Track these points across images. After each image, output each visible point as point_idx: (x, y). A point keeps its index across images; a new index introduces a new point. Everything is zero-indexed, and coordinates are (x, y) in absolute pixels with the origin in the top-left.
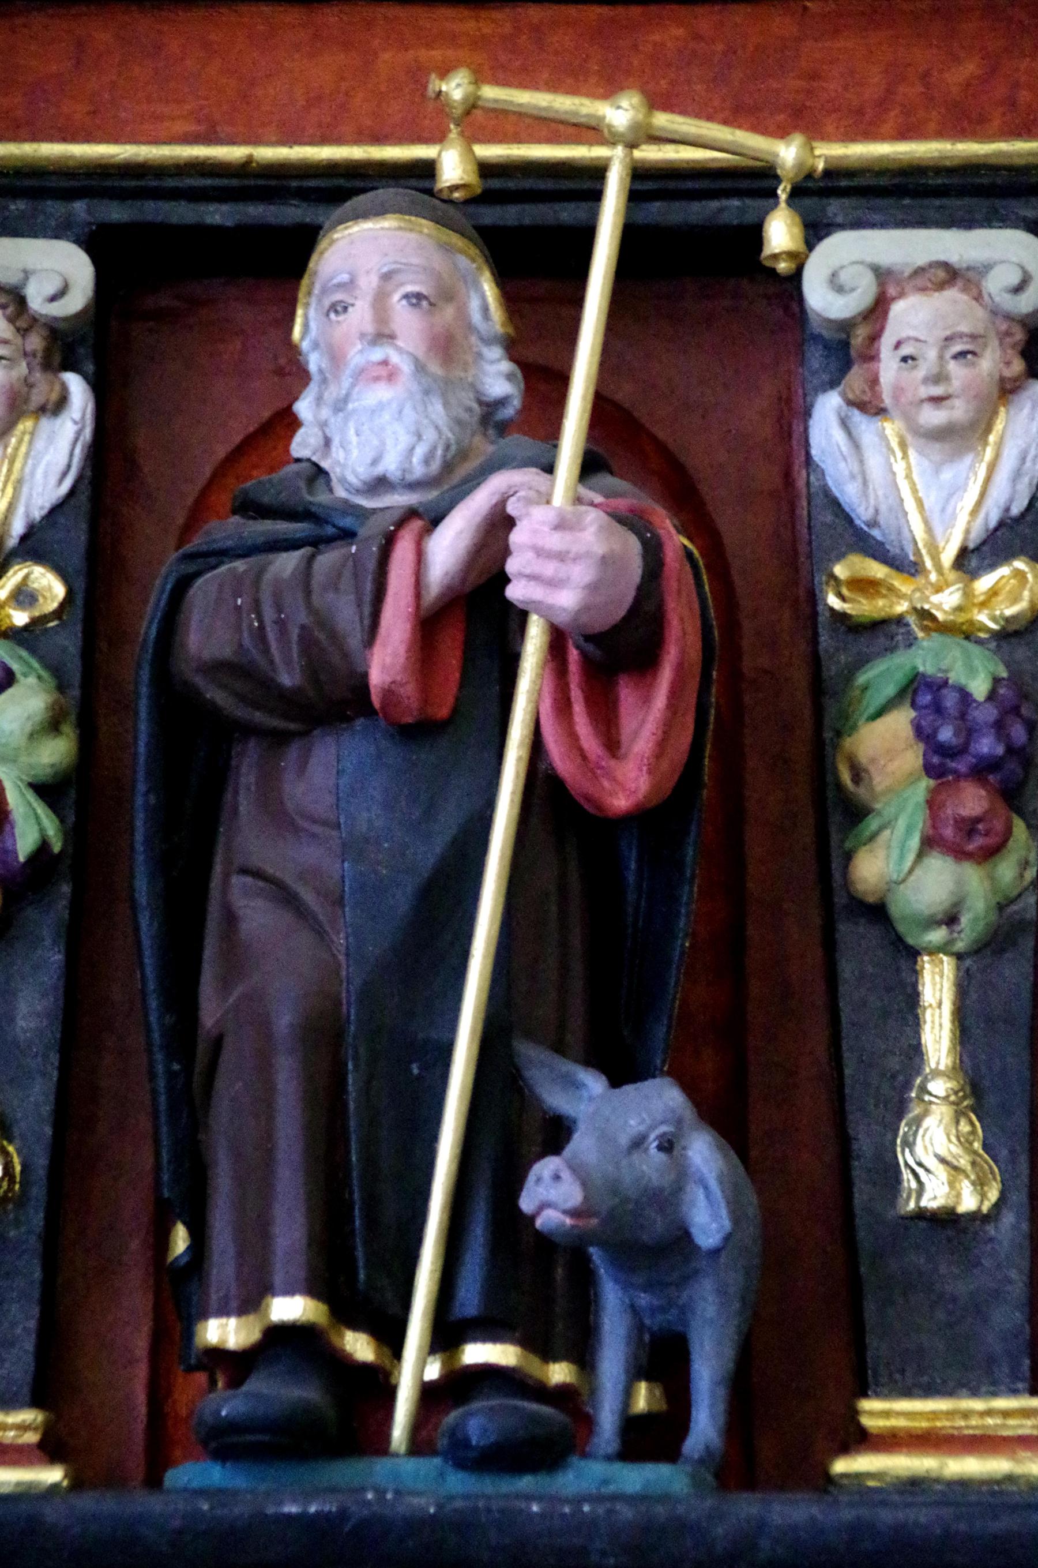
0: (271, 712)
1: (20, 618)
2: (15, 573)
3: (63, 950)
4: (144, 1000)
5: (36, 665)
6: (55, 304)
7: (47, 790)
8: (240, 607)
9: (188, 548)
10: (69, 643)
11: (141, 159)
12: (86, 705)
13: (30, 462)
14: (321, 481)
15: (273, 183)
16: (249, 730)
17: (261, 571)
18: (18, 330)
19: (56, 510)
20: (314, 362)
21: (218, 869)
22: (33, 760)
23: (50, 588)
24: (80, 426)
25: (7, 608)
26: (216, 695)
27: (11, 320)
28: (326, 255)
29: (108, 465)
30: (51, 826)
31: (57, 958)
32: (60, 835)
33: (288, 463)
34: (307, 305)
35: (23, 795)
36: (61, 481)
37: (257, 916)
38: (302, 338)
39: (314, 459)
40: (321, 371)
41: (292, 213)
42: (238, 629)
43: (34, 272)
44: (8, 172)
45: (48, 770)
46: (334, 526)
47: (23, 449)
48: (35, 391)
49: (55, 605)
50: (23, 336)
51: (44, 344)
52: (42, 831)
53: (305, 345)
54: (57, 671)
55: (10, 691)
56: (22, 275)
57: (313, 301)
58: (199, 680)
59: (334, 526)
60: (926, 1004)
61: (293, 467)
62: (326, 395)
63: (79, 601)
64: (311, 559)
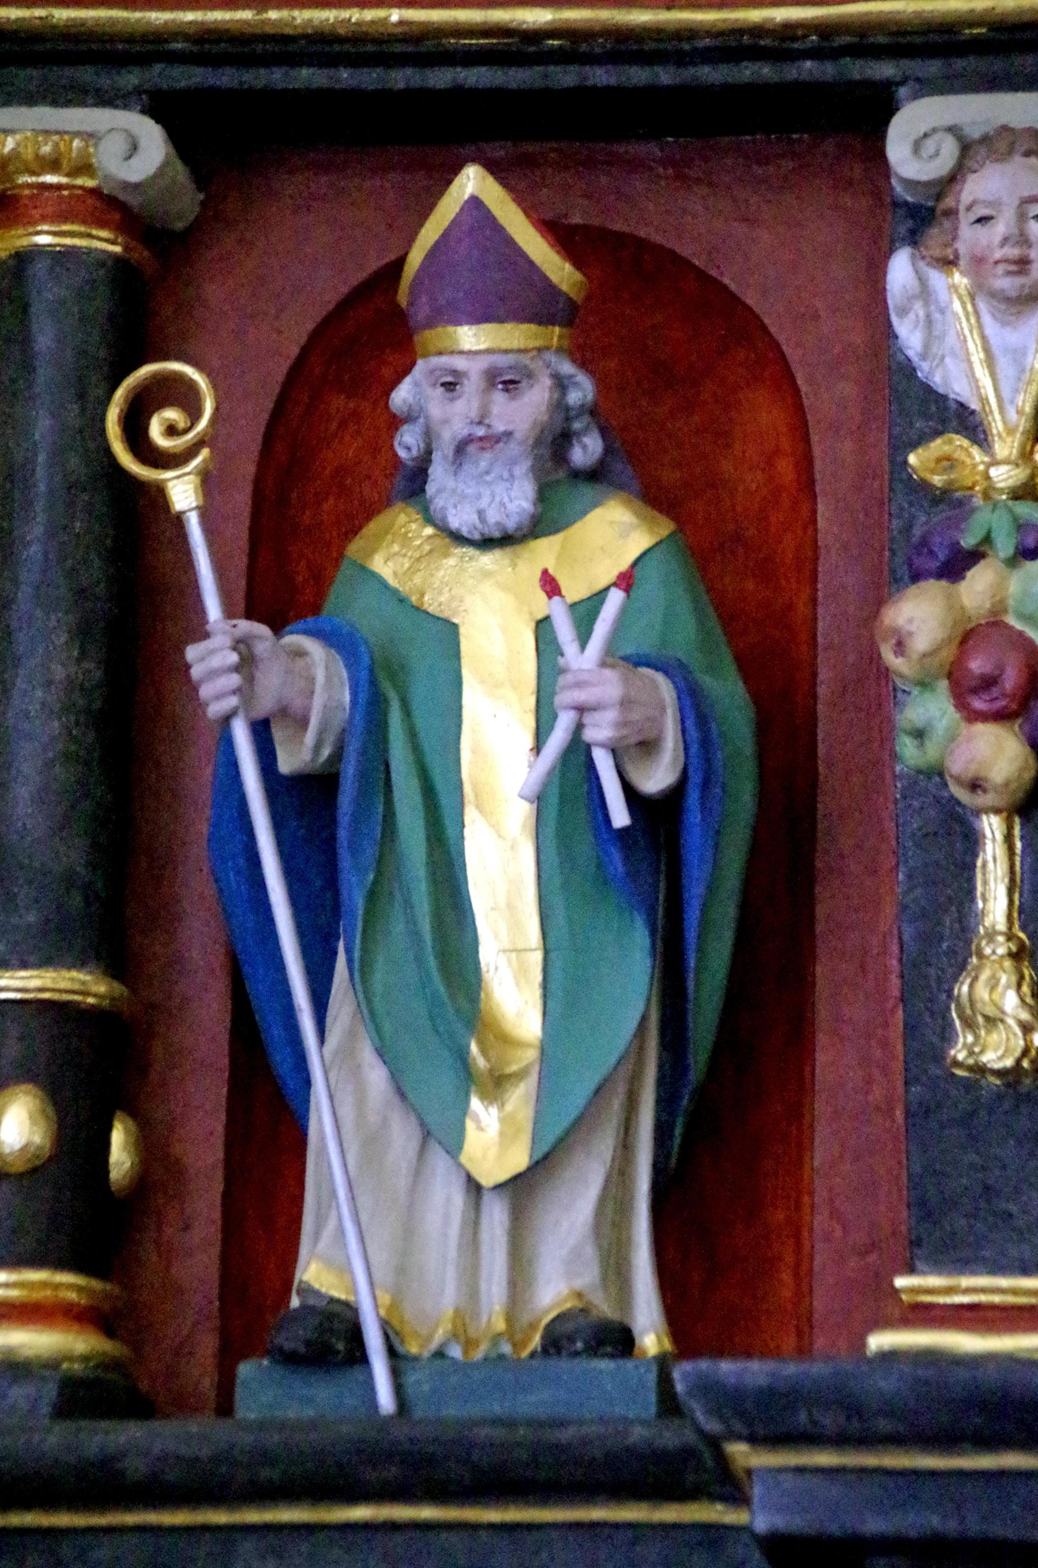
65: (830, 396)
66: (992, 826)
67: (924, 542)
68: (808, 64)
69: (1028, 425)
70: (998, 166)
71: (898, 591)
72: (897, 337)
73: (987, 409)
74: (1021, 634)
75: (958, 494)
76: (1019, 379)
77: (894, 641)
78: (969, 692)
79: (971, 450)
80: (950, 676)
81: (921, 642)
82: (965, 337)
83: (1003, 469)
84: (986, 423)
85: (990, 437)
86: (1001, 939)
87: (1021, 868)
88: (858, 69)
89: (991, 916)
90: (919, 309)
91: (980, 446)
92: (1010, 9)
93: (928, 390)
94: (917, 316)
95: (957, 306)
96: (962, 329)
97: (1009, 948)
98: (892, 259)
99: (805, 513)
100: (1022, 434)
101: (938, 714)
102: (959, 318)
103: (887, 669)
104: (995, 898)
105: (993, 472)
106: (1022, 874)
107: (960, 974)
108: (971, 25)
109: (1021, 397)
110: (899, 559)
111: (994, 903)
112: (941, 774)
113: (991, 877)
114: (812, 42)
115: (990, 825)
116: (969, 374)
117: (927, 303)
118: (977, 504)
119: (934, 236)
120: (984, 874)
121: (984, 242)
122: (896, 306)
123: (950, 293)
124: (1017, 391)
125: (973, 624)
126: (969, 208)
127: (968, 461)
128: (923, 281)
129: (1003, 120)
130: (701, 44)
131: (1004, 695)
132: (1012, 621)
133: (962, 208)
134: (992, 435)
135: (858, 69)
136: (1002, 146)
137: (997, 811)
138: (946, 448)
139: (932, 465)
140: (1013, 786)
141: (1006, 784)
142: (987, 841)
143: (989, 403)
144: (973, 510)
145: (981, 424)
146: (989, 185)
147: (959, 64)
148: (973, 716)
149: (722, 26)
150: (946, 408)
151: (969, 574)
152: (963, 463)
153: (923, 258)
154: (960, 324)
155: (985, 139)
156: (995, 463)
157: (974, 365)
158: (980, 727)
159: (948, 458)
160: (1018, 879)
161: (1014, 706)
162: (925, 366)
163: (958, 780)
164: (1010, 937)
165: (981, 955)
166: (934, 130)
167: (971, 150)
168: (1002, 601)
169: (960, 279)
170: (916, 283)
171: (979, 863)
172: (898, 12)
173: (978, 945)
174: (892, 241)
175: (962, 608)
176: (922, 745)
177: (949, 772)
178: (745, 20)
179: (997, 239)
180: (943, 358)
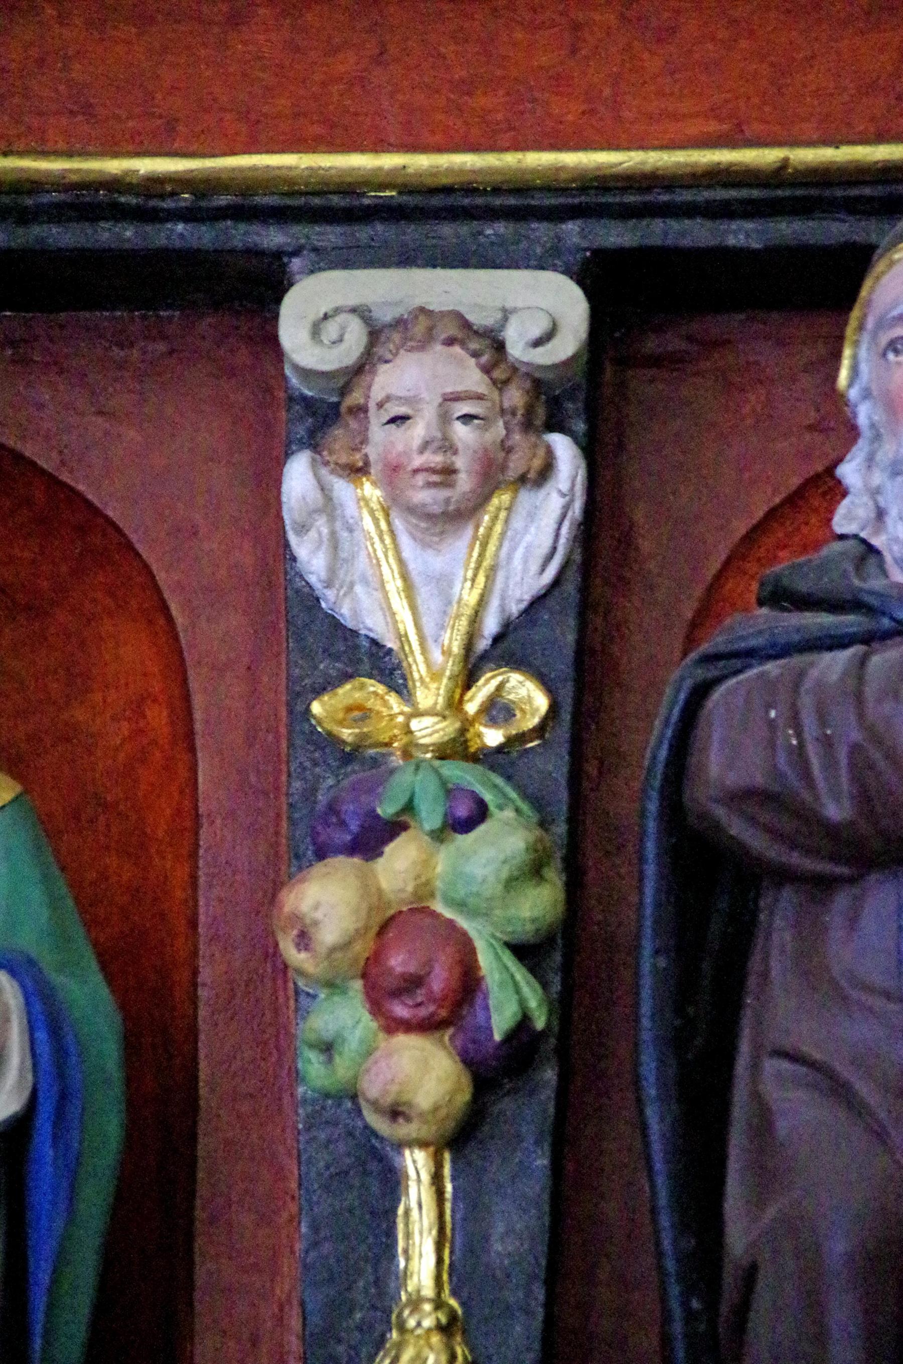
0: (809, 851)
1: (493, 737)
2: (488, 681)
3: (548, 1154)
4: (654, 1221)
5: (513, 795)
6: (540, 350)
7: (526, 952)
8: (773, 720)
9: (705, 648)
10: (555, 766)
11: (648, 168)
12: (576, 849)
13: (374, 561)
14: (872, 560)
15: (814, 192)
16: (784, 876)
17: (801, 675)
18: (494, 382)
19: (538, 601)
20: (864, 414)
21: (745, 1047)
22: (512, 912)
23: (530, 699)
24: (567, 498)
25: (477, 725)
26: (737, 828)
27: (487, 370)
28: (885, 280)
29: (600, 539)
30: (534, 999)
31: (542, 1161)
32: (545, 1010)
33: (826, 542)
34: (856, 344)
35: (498, 958)
36: (543, 569)
37: (797, 1109)
38: (850, 385)
39: (863, 535)
40: (873, 426)
41: (834, 230)
42: (772, 745)
43: (515, 310)
44: (485, 190)
45: (529, 927)
46: (893, 619)
47: (498, 528)
48: (514, 457)
49: (534, 721)
50: (500, 390)
51: (526, 398)
52: (522, 1002)
53: (853, 394)
54: (538, 802)
55: (482, 828)
56: (499, 315)
57: (866, 338)
58: (720, 812)
59: (893, 619)
60: (748, 990)
61: (837, 546)
62: (879, 456)
63: (566, 716)
64: (863, 661)
65: (212, 633)
66: (416, 1164)
67: (332, 808)
68: (180, 227)
69: (456, 668)
70: (415, 356)
71: (300, 869)
72: (294, 559)
73: (407, 648)
74: (451, 923)
75: (372, 751)
76: (445, 612)
77: (295, 932)
78: (386, 994)
79: (387, 697)
80: (364, 976)
81: (329, 935)
82: (377, 559)
83: (428, 721)
84: (405, 664)
85: (410, 683)
86: (427, 1307)
87: (453, 1217)
88: (242, 235)
89: (415, 1278)
90: (321, 525)
91: (398, 692)
92: (424, 168)
93: (335, 625)
94: (320, 534)
95: (368, 523)
96: (375, 551)
97: (438, 1319)
98: (287, 466)
99: (183, 773)
100: (450, 678)
101: (350, 1023)
102: (371, 538)
103: (286, 966)
104: (421, 1255)
105: (415, 724)
106: (453, 1224)
107: (376, 1354)
108: (383, 186)
109: (448, 635)
110: (301, 831)
111: (420, 1261)
112: (354, 1097)
113: (415, 1228)
114: (185, 199)
115: (414, 1162)
116: (384, 606)
117: (332, 519)
118: (395, 764)
119: (338, 435)
120: (407, 1225)
121: (400, 447)
122: (294, 522)
123: (360, 508)
124: (443, 627)
125: (392, 912)
126: (380, 405)
127: (385, 712)
128: (323, 488)
129: (418, 302)
130: (45, 199)
131: (431, 998)
132: (439, 907)
133: (372, 405)
134: (414, 681)
135: (242, 235)
136: (419, 329)
137: (423, 1144)
138: (357, 695)
139: (341, 715)
140: (443, 1112)
141: (436, 1109)
142: (410, 1183)
143: (408, 641)
144: (392, 772)
145: (399, 666)
146: (405, 377)
147: (363, 233)
148: (395, 1026)
149: (74, 178)
150: (357, 647)
151: (388, 849)
152: (378, 713)
153: (327, 463)
154: (372, 544)
155: (400, 323)
156: (418, 714)
157: (390, 595)
158: (402, 1039)
159: (360, 707)
160: (449, 1226)
161: (443, 1013)
162: (330, 594)
163: (375, 1105)
164: (439, 1304)
165: (402, 1329)
166: (337, 311)
167: (383, 336)
168: (427, 883)
169: (371, 491)
170: (319, 495)
171: (401, 1211)
172: (290, 168)
173: (400, 1315)
174: (288, 445)
175: (380, 891)
176: (330, 1060)
177: (364, 1094)
178: (100, 171)
179: (416, 443)
180: (352, 585)
